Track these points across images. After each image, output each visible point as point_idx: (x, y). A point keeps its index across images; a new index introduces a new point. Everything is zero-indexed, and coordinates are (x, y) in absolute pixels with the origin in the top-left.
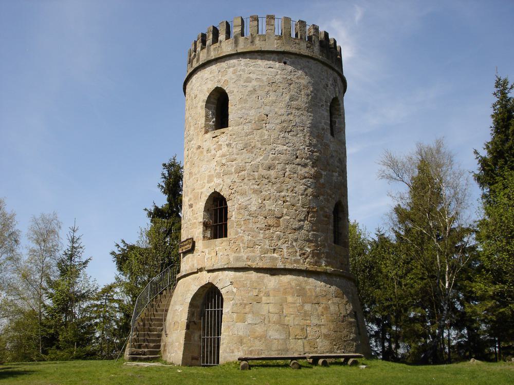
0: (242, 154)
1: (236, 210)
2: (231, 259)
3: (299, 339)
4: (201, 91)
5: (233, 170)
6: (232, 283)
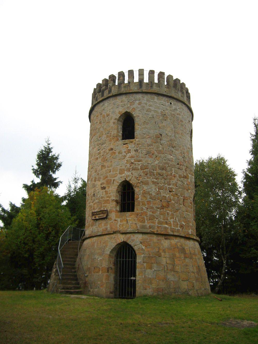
0: (145, 157)
1: (141, 194)
2: (139, 227)
3: (185, 281)
4: (114, 112)
5: (139, 168)
6: (141, 243)
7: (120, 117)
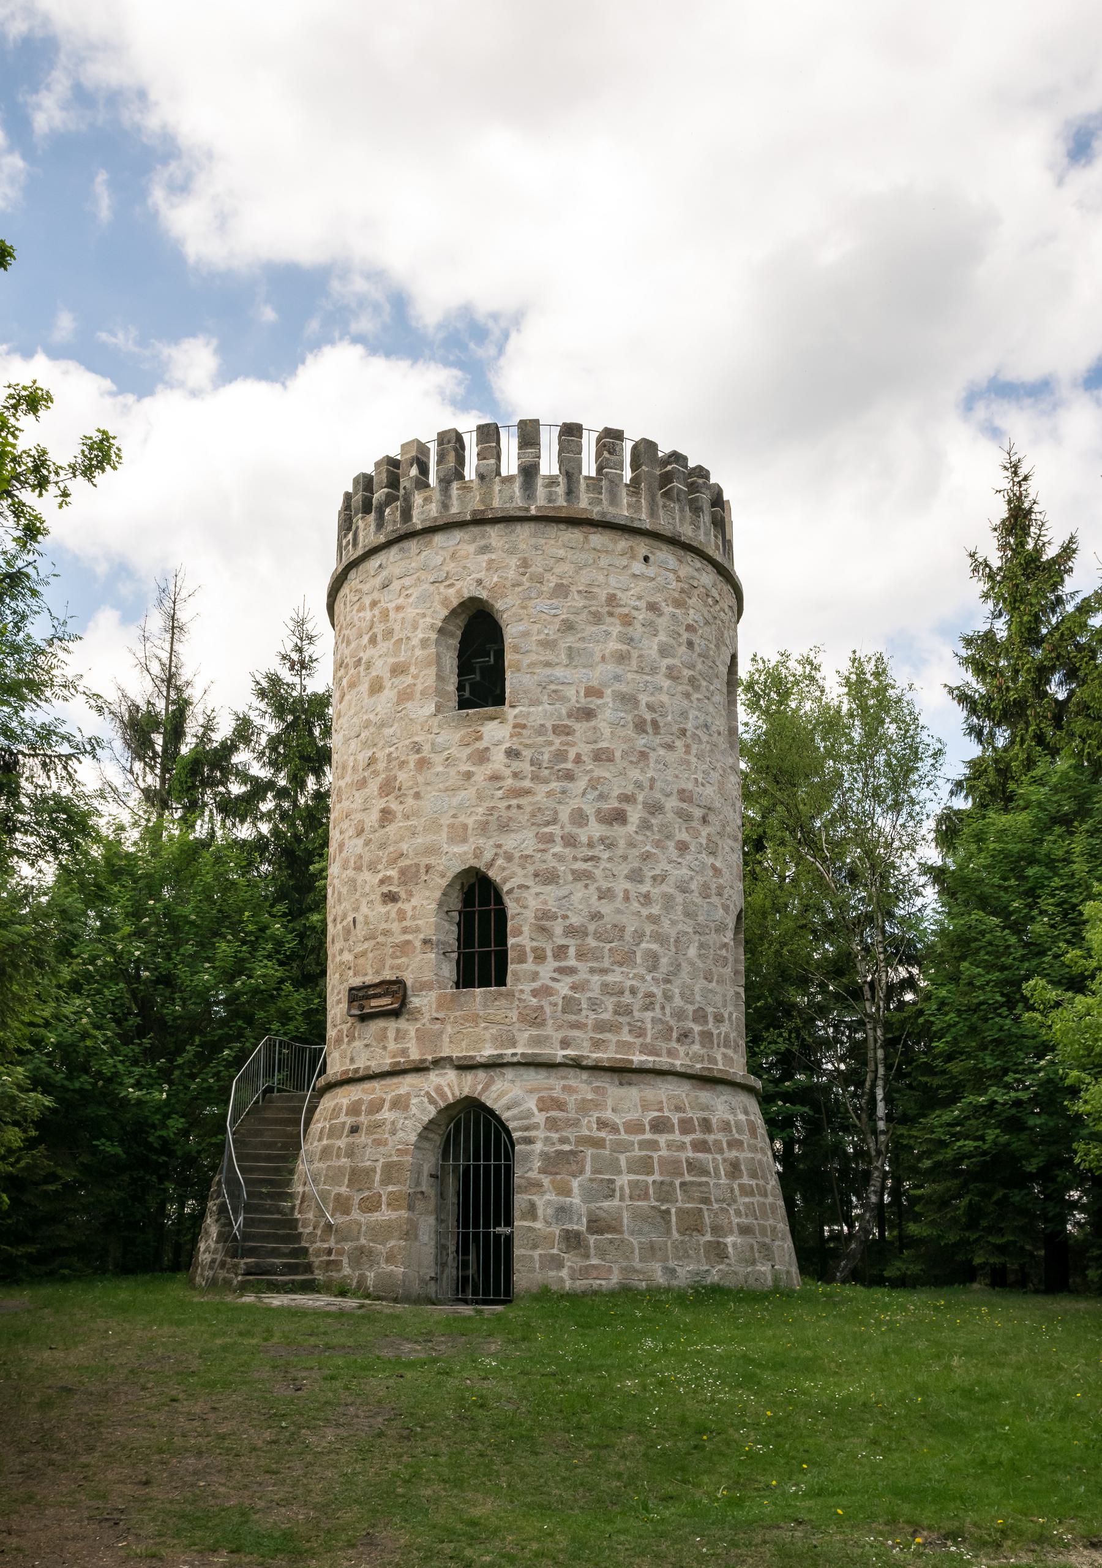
7: (446, 620)
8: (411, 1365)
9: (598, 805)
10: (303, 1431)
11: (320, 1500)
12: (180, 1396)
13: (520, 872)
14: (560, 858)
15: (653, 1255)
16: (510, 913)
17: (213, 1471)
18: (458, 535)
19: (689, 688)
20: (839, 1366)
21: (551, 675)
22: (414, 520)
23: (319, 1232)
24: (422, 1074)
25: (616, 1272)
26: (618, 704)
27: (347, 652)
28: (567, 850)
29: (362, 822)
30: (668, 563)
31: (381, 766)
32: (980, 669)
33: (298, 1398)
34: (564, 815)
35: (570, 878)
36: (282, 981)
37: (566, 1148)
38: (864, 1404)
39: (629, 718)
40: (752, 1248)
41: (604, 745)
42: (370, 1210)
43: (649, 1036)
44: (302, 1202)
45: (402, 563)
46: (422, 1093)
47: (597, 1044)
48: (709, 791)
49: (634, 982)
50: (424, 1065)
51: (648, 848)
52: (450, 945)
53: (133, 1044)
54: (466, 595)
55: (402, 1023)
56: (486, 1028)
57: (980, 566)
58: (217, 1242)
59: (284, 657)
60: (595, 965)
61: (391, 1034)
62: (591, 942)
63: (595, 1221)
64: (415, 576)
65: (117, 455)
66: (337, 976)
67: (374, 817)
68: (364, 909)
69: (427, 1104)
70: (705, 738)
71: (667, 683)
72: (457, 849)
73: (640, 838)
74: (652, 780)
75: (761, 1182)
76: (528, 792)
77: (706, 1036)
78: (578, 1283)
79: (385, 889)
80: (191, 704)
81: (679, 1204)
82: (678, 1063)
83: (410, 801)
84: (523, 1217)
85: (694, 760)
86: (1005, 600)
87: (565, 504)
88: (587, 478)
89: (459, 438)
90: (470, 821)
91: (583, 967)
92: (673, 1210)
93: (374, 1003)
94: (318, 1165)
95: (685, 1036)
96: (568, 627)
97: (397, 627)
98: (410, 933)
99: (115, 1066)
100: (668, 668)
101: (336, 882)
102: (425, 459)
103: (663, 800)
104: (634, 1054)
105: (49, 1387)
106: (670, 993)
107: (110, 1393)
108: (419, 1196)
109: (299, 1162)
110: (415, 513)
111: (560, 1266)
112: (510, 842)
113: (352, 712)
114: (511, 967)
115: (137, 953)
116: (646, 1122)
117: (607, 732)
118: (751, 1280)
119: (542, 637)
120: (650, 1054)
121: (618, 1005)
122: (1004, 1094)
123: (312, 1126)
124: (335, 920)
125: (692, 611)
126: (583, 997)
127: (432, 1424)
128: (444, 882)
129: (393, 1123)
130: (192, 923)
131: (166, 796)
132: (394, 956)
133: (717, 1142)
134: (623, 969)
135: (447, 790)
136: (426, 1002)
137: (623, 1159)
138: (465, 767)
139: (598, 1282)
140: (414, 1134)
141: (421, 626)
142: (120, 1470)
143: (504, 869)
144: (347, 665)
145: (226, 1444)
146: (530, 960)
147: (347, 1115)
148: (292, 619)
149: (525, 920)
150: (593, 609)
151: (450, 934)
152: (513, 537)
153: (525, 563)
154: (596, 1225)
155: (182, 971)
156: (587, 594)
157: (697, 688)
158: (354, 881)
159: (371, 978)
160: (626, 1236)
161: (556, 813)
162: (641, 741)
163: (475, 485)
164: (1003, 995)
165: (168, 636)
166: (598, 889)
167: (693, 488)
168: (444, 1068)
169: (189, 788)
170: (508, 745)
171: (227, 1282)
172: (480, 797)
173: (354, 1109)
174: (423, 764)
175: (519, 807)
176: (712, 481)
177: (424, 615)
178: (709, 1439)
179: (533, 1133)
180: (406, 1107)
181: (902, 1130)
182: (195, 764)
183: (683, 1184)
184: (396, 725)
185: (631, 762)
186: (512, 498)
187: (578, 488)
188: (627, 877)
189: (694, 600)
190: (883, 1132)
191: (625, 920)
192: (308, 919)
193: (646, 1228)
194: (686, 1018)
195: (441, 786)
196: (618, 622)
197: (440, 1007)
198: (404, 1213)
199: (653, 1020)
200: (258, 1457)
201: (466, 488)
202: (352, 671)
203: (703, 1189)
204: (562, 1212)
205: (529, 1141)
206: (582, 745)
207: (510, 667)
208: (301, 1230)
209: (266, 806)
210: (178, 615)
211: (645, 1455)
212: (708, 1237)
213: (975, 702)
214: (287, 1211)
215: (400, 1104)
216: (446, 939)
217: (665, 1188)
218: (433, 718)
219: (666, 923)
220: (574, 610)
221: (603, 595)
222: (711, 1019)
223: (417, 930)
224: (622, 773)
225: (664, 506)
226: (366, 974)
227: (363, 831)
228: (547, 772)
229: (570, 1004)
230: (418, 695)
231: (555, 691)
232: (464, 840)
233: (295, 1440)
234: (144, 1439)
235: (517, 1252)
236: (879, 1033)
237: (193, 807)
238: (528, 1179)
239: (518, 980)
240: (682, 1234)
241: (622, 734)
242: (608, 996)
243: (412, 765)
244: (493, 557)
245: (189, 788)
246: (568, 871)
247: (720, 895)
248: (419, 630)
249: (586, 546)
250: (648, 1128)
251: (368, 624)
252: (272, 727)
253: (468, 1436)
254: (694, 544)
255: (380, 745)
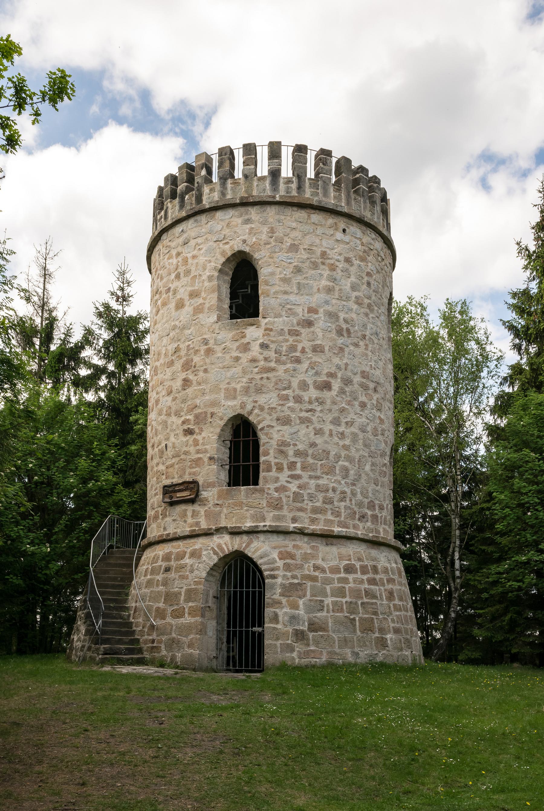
7: (224, 264)
8: (224, 709)
9: (314, 378)
10: (172, 750)
11: (197, 795)
12: (89, 728)
13: (268, 417)
14: (292, 409)
15: (346, 645)
16: (261, 442)
17: (124, 776)
18: (231, 212)
19: (368, 311)
20: (475, 710)
21: (288, 299)
22: (204, 202)
23: (146, 630)
24: (209, 537)
25: (325, 654)
26: (327, 318)
27: (161, 284)
28: (297, 405)
29: (171, 387)
30: (356, 234)
31: (183, 353)
32: (520, 310)
33: (164, 729)
34: (295, 384)
35: (298, 422)
36: (116, 484)
37: (296, 581)
38: (503, 734)
39: (334, 327)
40: (401, 641)
41: (319, 342)
42: (178, 617)
43: (343, 516)
44: (134, 612)
45: (196, 229)
46: (209, 548)
47: (313, 521)
48: (378, 373)
49: (334, 485)
50: (210, 532)
51: (343, 405)
52: (225, 461)
53: (28, 519)
54: (236, 249)
55: (196, 507)
56: (247, 510)
57: (523, 250)
58: (85, 635)
59: (112, 294)
60: (312, 474)
61: (189, 514)
62: (310, 460)
63: (313, 624)
64: (204, 237)
65: (72, 89)
66: (155, 479)
67: (179, 383)
68: (172, 439)
69: (212, 555)
70: (376, 341)
71: (355, 307)
72: (230, 403)
73: (339, 399)
74: (346, 364)
75: (405, 603)
76: (273, 370)
77: (375, 518)
78: (303, 660)
79: (186, 427)
80: (58, 320)
81: (360, 615)
82: (359, 533)
83: (201, 374)
84: (271, 622)
85: (370, 354)
86: (537, 270)
87: (296, 195)
88: (310, 179)
89: (232, 152)
90: (238, 387)
91: (305, 475)
92: (357, 619)
93: (179, 495)
94: (144, 590)
95: (363, 517)
96: (298, 270)
97: (193, 269)
98: (201, 453)
99: (18, 532)
100: (356, 297)
101: (154, 423)
102: (210, 165)
103: (352, 377)
104: (334, 527)
105: (4, 722)
106: (355, 492)
107: (44, 726)
108: (207, 609)
109: (132, 589)
110: (205, 198)
111: (292, 650)
112: (262, 399)
113: (165, 320)
114: (262, 474)
115: (31, 465)
116: (341, 567)
117: (320, 335)
118: (400, 660)
119: (282, 276)
120: (344, 527)
121: (325, 498)
122: (538, 555)
123: (139, 568)
124: (153, 446)
125: (370, 264)
126: (305, 493)
127: (251, 745)
128: (222, 423)
129: (192, 566)
130: (63, 448)
131: (42, 375)
132: (191, 467)
133: (381, 579)
134: (329, 477)
135: (224, 367)
136: (211, 494)
137: (328, 588)
138: (235, 354)
139: (315, 660)
140: (205, 572)
141: (208, 268)
142: (64, 776)
143: (258, 415)
144: (161, 292)
145: (127, 758)
146: (274, 470)
147: (162, 561)
148: (118, 271)
149: (271, 446)
150: (313, 260)
151: (225, 453)
152: (265, 214)
153: (272, 231)
154: (314, 627)
155: (58, 477)
156: (309, 250)
157: (372, 311)
158: (166, 422)
159: (176, 481)
160: (331, 633)
161: (290, 382)
162: (340, 341)
163: (242, 181)
164: (538, 499)
165: (43, 279)
166: (314, 429)
167: (371, 189)
168: (222, 533)
169: (56, 370)
170: (261, 341)
171: (92, 659)
172: (244, 372)
173: (167, 558)
174: (209, 352)
175: (268, 378)
176: (382, 186)
177: (210, 261)
178: (419, 755)
179: (276, 573)
180: (200, 557)
181: (469, 576)
182: (61, 355)
183: (362, 604)
184: (192, 328)
185: (334, 353)
186: (264, 190)
187: (304, 185)
188: (331, 422)
189: (371, 257)
190: (458, 577)
191: (330, 448)
192: (128, 449)
193: (342, 629)
194: (364, 506)
195: (220, 365)
196: (327, 268)
197: (219, 497)
198: (199, 619)
199: (345, 507)
200: (149, 766)
201: (236, 183)
202: (164, 296)
203: (374, 606)
204: (294, 619)
205: (274, 577)
206: (306, 342)
207: (262, 293)
208: (134, 628)
209: (103, 381)
210: (48, 267)
211: (384, 764)
212: (377, 635)
213: (518, 330)
214: (126, 617)
215: (195, 554)
216: (223, 457)
217: (353, 606)
218: (216, 324)
219: (353, 450)
220: (300, 260)
221: (318, 252)
222: (377, 507)
223: (206, 451)
224: (329, 360)
225: (355, 199)
226: (173, 478)
227: (171, 392)
228: (284, 358)
229: (297, 497)
230: (206, 310)
231: (290, 309)
232: (235, 398)
233: (169, 756)
234: (74, 755)
235: (267, 642)
236: (457, 521)
237: (57, 384)
238: (273, 599)
239: (267, 482)
240: (362, 632)
241: (329, 336)
242: (319, 492)
243: (202, 352)
244: (253, 226)
245: (56, 370)
246: (297, 417)
247: (383, 435)
248: (207, 270)
249: (309, 222)
250: (342, 570)
251: (175, 267)
252: (106, 335)
253: (274, 753)
254: (372, 223)
255: (182, 340)
